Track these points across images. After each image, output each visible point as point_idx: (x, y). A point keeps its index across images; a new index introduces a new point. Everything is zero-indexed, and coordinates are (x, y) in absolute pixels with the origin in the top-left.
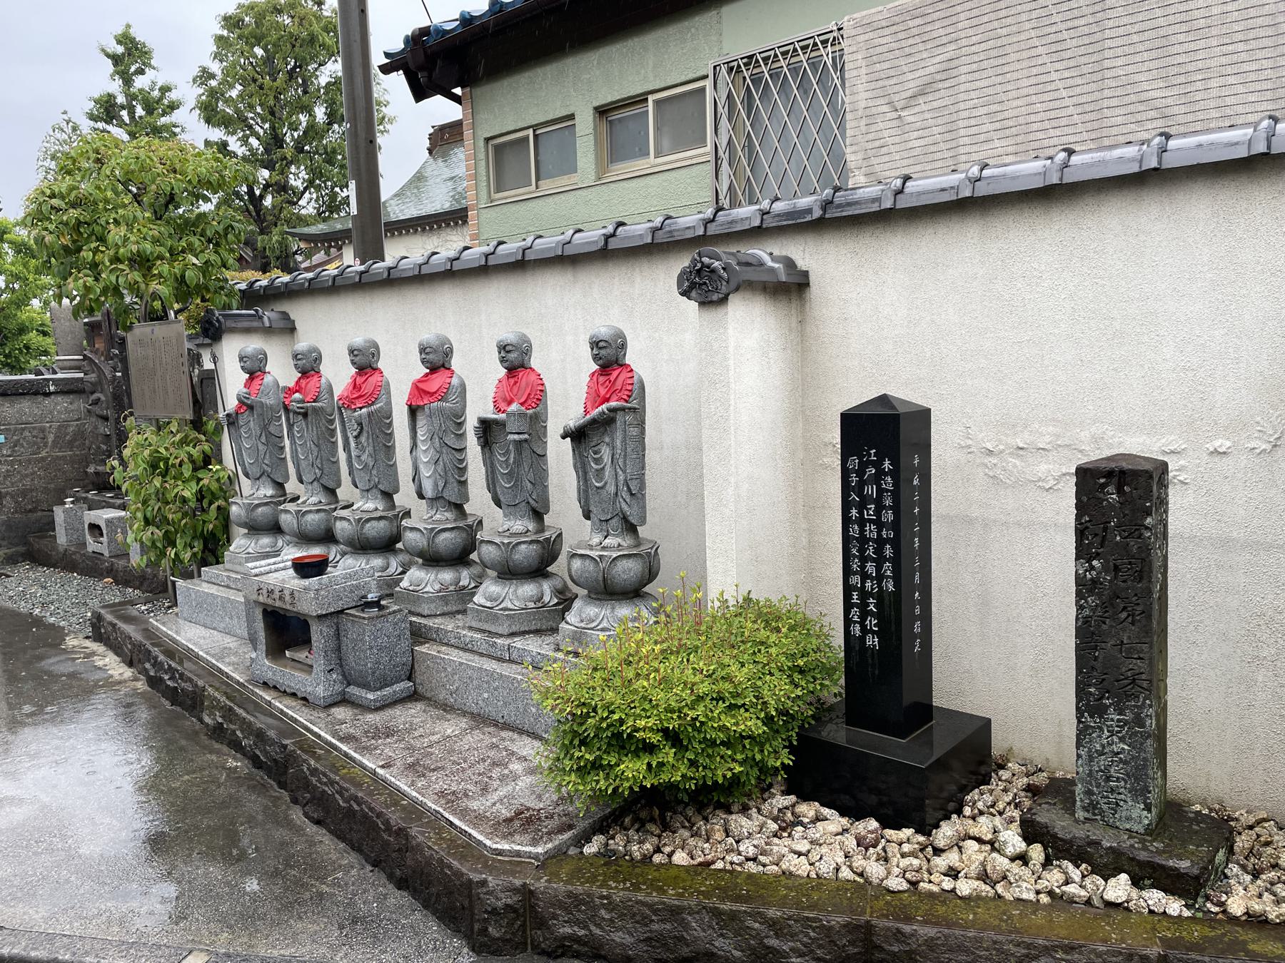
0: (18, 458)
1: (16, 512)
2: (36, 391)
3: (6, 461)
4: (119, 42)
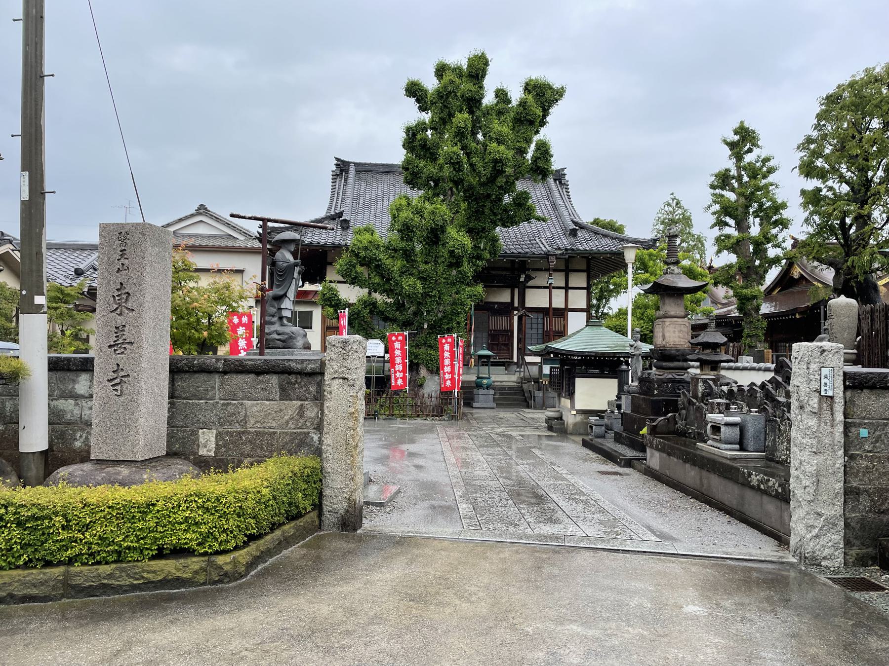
0: (878, 455)
3: (866, 456)
4: (736, 133)
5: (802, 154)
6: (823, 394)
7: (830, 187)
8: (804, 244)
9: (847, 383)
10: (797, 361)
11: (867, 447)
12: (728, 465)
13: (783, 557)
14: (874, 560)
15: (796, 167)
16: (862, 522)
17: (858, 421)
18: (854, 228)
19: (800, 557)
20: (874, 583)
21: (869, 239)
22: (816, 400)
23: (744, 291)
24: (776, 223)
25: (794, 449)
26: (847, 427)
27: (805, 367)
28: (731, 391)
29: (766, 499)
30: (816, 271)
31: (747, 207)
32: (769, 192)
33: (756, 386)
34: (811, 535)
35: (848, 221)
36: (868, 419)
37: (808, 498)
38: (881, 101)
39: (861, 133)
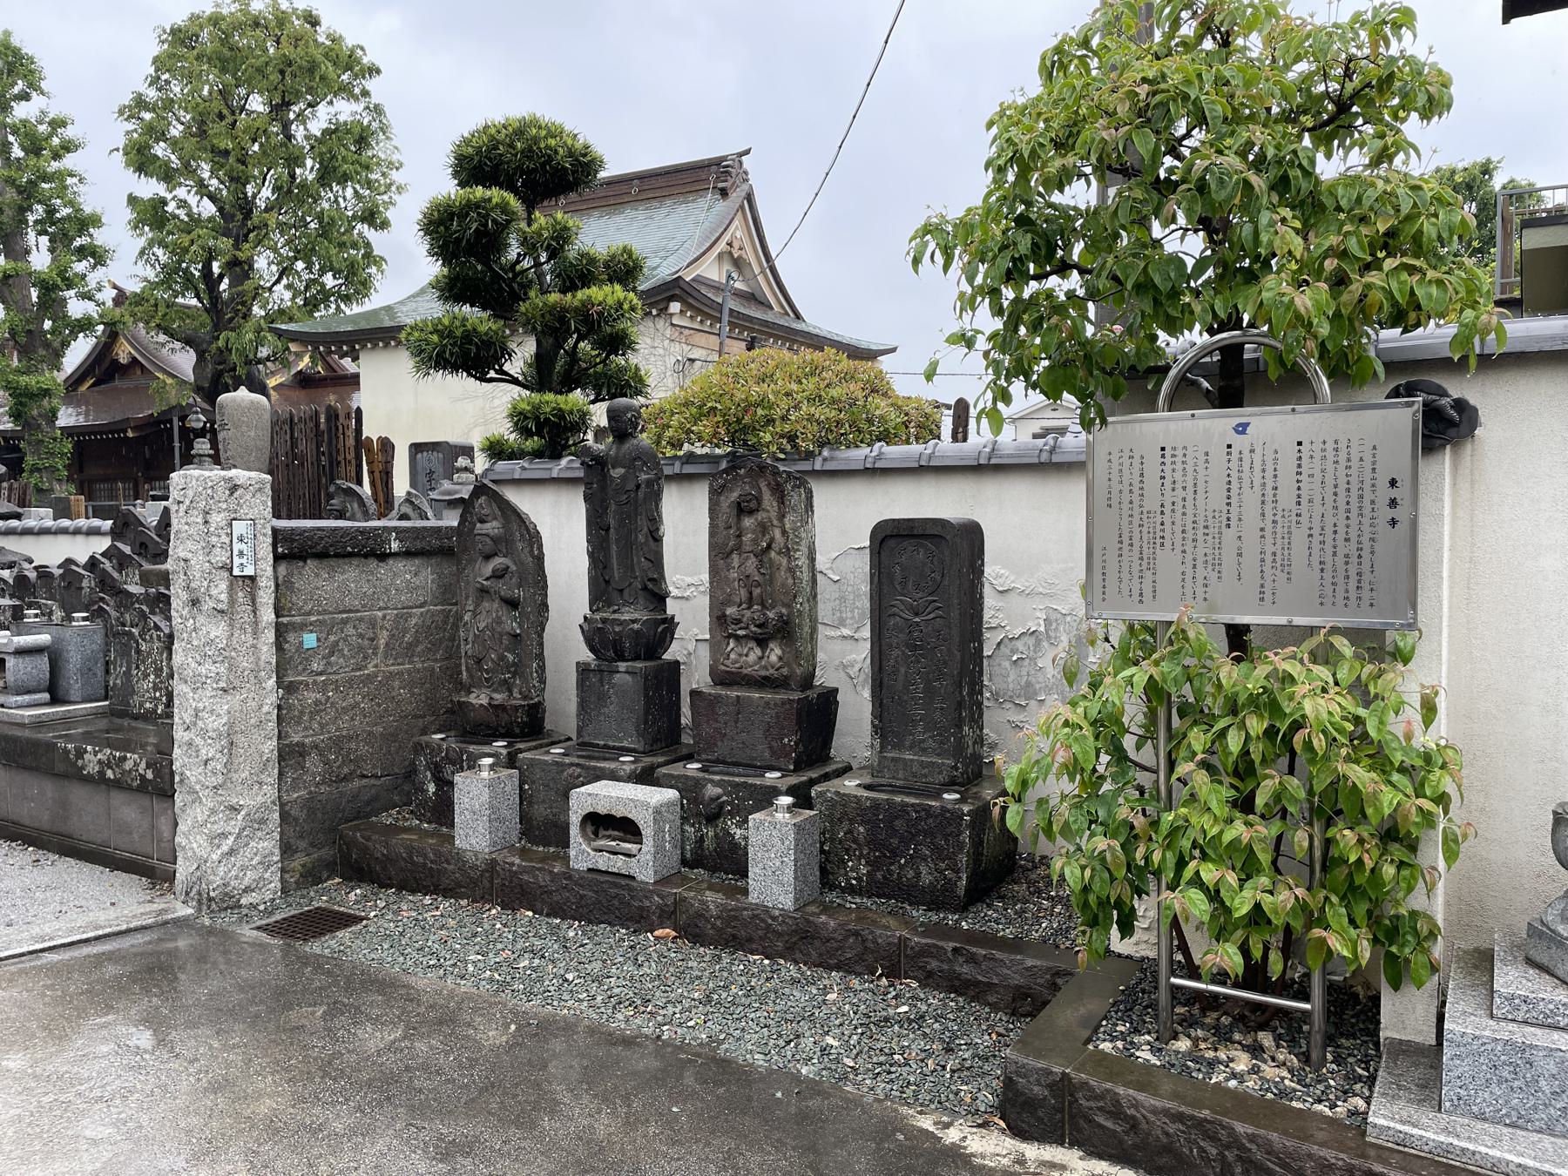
1: (323, 782)
2: (370, 550)
3: (315, 682)
5: (130, 127)
6: (236, 572)
7: (181, 201)
8: (139, 299)
9: (280, 550)
10: (183, 508)
11: (315, 666)
12: (28, 741)
13: (165, 911)
14: (331, 868)
15: (117, 150)
16: (310, 804)
17: (298, 619)
18: (226, 280)
19: (199, 902)
20: (338, 912)
21: (252, 305)
22: (223, 586)
23: (24, 380)
24: (82, 252)
25: (179, 688)
26: (281, 631)
27: (200, 520)
28: (21, 579)
29: (118, 798)
30: (164, 351)
31: (23, 210)
32: (66, 188)
33: (77, 565)
34: (219, 852)
35: (216, 268)
36: (319, 613)
37: (213, 781)
38: (267, 64)
39: (233, 113)
